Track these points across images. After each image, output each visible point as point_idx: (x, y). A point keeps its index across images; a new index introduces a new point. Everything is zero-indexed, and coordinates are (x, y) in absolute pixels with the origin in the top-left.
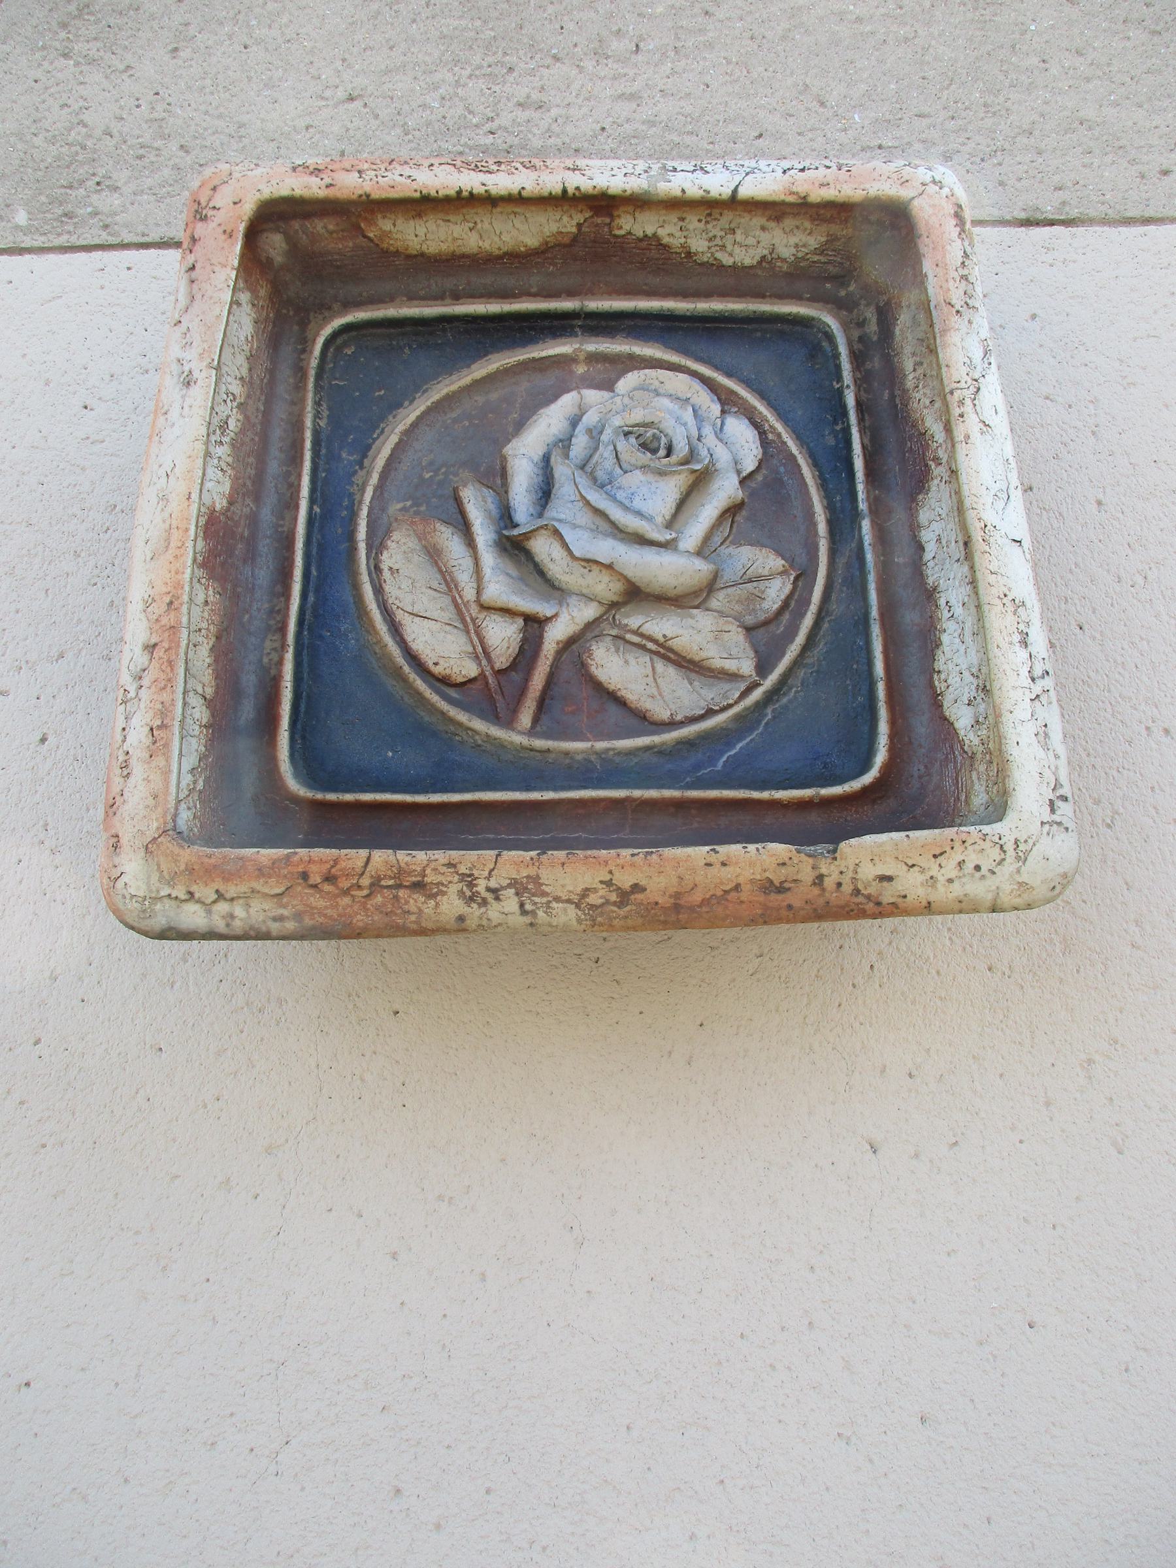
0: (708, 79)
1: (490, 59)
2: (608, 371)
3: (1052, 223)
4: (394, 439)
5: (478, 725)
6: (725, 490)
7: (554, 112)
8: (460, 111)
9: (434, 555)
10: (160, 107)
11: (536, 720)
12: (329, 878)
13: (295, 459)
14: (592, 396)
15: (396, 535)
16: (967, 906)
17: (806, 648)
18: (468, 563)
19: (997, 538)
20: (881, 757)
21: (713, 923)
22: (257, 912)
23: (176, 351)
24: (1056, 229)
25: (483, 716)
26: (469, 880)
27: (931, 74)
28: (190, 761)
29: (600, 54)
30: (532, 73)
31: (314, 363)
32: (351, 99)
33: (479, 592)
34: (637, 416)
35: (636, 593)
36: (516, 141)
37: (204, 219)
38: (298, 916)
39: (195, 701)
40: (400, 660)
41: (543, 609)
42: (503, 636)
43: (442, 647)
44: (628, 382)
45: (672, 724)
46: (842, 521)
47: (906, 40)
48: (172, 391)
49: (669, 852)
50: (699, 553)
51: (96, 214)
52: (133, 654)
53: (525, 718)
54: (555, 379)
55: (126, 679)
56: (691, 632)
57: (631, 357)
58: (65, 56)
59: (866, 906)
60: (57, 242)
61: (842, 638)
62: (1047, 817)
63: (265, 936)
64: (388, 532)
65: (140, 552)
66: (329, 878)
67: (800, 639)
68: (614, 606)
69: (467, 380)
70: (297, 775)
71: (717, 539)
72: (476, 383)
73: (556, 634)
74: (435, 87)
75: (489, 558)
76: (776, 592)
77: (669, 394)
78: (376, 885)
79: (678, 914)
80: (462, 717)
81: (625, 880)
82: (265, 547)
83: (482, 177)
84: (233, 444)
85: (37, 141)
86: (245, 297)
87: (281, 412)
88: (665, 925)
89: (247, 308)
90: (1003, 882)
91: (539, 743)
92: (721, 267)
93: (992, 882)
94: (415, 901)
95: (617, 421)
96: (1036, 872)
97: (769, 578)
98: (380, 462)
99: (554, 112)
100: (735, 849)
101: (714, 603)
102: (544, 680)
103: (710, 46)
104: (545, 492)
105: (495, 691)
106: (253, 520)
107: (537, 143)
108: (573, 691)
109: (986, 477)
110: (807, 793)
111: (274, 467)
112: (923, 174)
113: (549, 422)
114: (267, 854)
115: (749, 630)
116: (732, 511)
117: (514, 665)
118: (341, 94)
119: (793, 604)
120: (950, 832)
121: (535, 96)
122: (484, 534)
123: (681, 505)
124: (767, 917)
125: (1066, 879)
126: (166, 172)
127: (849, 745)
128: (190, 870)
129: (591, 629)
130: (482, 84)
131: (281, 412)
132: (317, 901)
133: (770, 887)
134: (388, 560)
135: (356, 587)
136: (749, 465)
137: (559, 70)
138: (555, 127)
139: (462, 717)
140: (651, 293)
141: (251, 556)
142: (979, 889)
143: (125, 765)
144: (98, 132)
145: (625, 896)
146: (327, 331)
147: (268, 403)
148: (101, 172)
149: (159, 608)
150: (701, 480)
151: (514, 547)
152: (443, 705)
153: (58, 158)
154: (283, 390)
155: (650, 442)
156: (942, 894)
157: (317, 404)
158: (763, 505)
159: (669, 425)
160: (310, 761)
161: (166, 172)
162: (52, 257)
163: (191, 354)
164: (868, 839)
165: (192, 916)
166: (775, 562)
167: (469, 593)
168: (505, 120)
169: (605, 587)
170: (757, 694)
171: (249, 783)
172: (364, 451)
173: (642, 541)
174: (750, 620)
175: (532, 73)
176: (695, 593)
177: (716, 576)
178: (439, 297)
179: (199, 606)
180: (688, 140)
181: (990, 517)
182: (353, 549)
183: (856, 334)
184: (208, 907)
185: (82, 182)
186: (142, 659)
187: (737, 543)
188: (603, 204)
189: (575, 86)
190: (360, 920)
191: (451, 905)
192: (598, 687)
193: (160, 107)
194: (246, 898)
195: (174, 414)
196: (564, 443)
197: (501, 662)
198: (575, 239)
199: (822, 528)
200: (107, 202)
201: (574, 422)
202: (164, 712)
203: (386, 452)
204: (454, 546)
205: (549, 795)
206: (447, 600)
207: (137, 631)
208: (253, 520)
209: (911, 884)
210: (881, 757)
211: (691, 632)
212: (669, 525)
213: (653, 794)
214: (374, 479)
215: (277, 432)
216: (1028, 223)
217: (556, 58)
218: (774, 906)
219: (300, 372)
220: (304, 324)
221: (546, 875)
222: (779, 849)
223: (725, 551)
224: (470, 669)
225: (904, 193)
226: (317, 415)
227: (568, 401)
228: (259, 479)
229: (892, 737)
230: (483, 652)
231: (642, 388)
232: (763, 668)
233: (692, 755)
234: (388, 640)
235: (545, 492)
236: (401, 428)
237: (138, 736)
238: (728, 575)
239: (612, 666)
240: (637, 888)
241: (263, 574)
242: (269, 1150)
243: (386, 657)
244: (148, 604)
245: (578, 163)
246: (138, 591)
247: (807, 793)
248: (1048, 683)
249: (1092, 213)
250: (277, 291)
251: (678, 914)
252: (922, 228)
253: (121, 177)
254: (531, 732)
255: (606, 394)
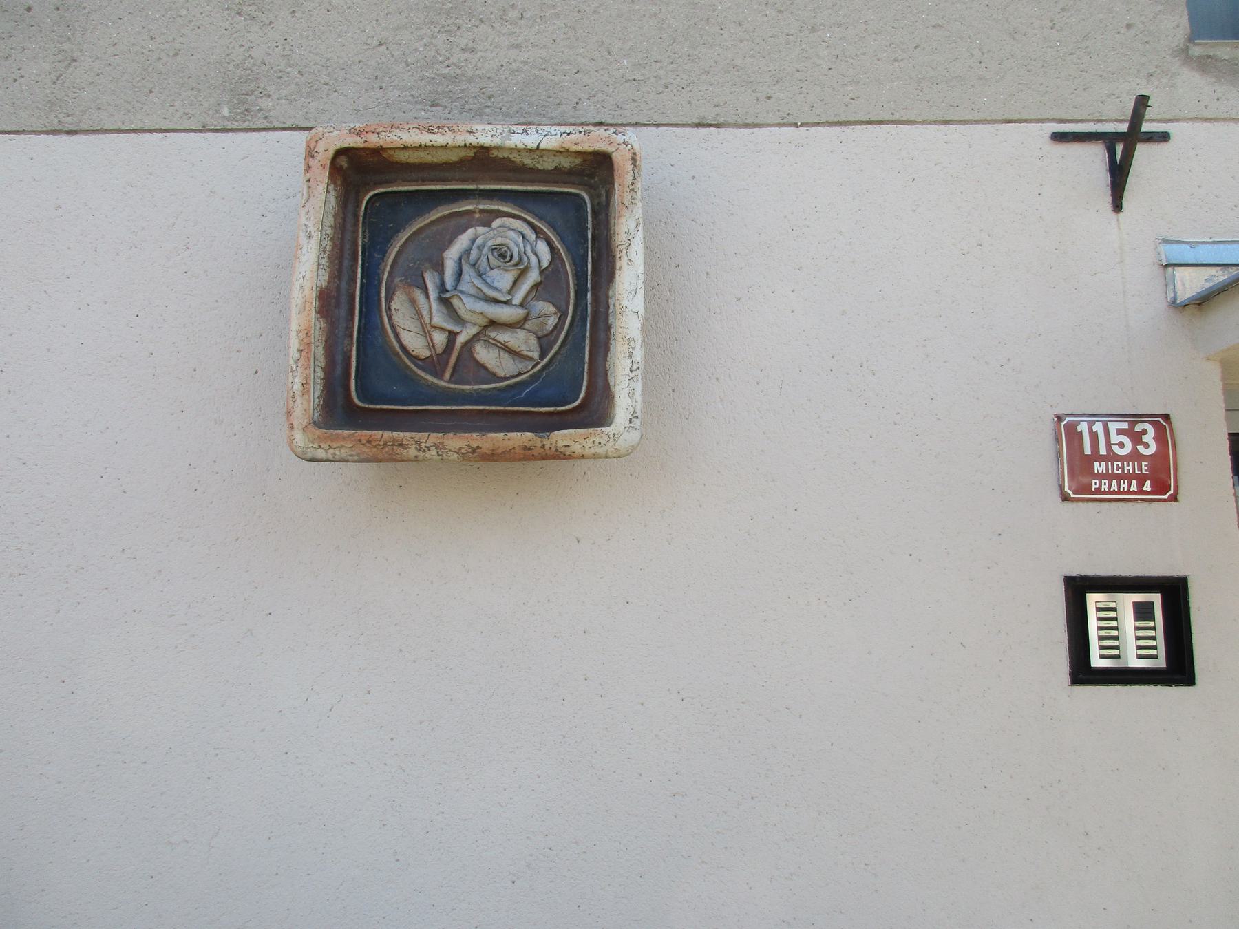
0: (554, 37)
1: (449, 21)
2: (487, 219)
3: (710, 125)
4: (396, 249)
5: (429, 377)
6: (533, 277)
7: (479, 54)
8: (433, 53)
9: (413, 302)
10: (288, 48)
11: (452, 375)
12: (369, 442)
13: (355, 260)
14: (481, 230)
15: (398, 294)
16: (595, 457)
17: (560, 348)
18: (426, 306)
19: (627, 312)
20: (582, 395)
21: (506, 460)
22: (344, 453)
23: (303, 220)
24: (712, 129)
25: (431, 374)
26: (419, 443)
27: (664, 36)
28: (318, 393)
29: (503, 19)
30: (469, 30)
31: (362, 213)
32: (381, 45)
33: (431, 319)
34: (499, 241)
35: (493, 324)
36: (460, 72)
37: (313, 156)
38: (358, 455)
39: (318, 369)
40: (398, 349)
41: (457, 329)
42: (440, 339)
43: (414, 342)
44: (496, 223)
45: (505, 379)
46: (581, 293)
47: (655, 15)
48: (303, 239)
49: (491, 435)
50: (521, 305)
51: (260, 110)
52: (294, 352)
53: (447, 376)
54: (463, 222)
55: (292, 362)
56: (516, 339)
57: (499, 211)
58: (239, 14)
59: (560, 455)
60: (245, 125)
61: (573, 343)
62: (627, 424)
63: (347, 461)
64: (394, 293)
65: (294, 311)
66: (369, 442)
67: (559, 343)
68: (485, 327)
69: (427, 221)
70: (358, 397)
71: (530, 298)
72: (432, 223)
73: (461, 339)
74: (421, 38)
75: (435, 305)
76: (552, 321)
77: (512, 230)
78: (385, 444)
79: (492, 457)
80: (422, 374)
81: (474, 445)
82: (344, 299)
83: (431, 137)
84: (329, 257)
85: (230, 67)
86: (331, 188)
87: (348, 236)
88: (489, 460)
89: (332, 193)
90: (609, 448)
91: (452, 386)
92: (538, 170)
93: (605, 448)
94: (399, 450)
95: (490, 243)
96: (622, 444)
97: (549, 315)
98: (390, 261)
99: (479, 54)
100: (514, 434)
101: (527, 326)
102: (456, 359)
103: (557, 16)
104: (459, 275)
105: (435, 364)
106: (338, 288)
107: (470, 73)
108: (467, 364)
109: (626, 285)
110: (552, 409)
111: (346, 263)
112: (620, 138)
113: (462, 241)
114: (347, 432)
115: (539, 338)
116: (536, 286)
117: (445, 351)
118: (376, 42)
119: (557, 328)
120: (591, 430)
121: (471, 45)
122: (433, 294)
123: (515, 283)
124: (527, 458)
125: (633, 448)
126: (293, 86)
127: (562, 394)
128: (319, 438)
129: (475, 338)
130: (444, 36)
131: (348, 236)
132: (365, 449)
133: (525, 448)
134: (394, 305)
135: (381, 317)
136: (545, 264)
137: (484, 28)
138: (479, 64)
139: (422, 374)
140: (508, 181)
141: (338, 305)
142: (600, 450)
143: (293, 397)
144: (259, 62)
145: (474, 450)
146: (367, 197)
147: (342, 234)
148: (262, 86)
149: (303, 335)
150: (523, 273)
151: (445, 302)
152: (415, 369)
153: (240, 77)
154: (349, 226)
155: (502, 254)
156: (587, 452)
157: (364, 232)
158: (549, 284)
159: (512, 245)
160: (363, 392)
161: (293, 86)
162: (241, 134)
163: (310, 224)
164: (561, 432)
165: (321, 454)
166: (550, 309)
167: (427, 320)
168: (454, 59)
169: (482, 321)
170: (539, 367)
171: (340, 400)
172: (384, 253)
173: (496, 301)
174: (540, 334)
175: (469, 30)
176: (519, 322)
177: (528, 315)
178: (415, 181)
179: (318, 328)
180: (543, 73)
181: (625, 303)
182: (380, 300)
183: (596, 201)
184: (326, 451)
185: (253, 92)
186: (297, 355)
187: (538, 300)
188: (482, 148)
189: (490, 39)
190: (380, 456)
191: (412, 452)
192: (477, 362)
193: (288, 48)
194: (339, 448)
195: (305, 249)
196: (467, 252)
197: (439, 351)
198: (473, 158)
199: (572, 294)
200: (266, 103)
201: (473, 241)
202: (307, 378)
203: (393, 255)
204: (421, 299)
205: (454, 408)
206: (417, 323)
207: (295, 344)
208: (338, 288)
209: (576, 448)
210: (582, 395)
211: (516, 339)
212: (510, 292)
213: (493, 408)
214: (388, 269)
215: (347, 246)
216: (699, 125)
217: (482, 21)
218: (527, 455)
219: (356, 216)
220: (357, 193)
221: (446, 442)
222: (529, 435)
223: (532, 303)
224: (427, 353)
225: (610, 149)
226: (364, 237)
227: (470, 233)
228: (340, 270)
229: (588, 387)
230: (432, 345)
231: (502, 226)
232: (542, 356)
233: (513, 392)
234: (393, 340)
235: (459, 275)
236: (399, 244)
237: (297, 387)
238: (533, 314)
239: (483, 354)
240: (478, 447)
241: (343, 312)
242: (353, 537)
243: (392, 348)
244: (298, 332)
245: (474, 128)
246: (294, 327)
247: (552, 409)
248: (639, 372)
249: (730, 121)
250: (345, 179)
251: (492, 457)
252: (616, 166)
253: (271, 89)
254: (450, 381)
255: (486, 229)
